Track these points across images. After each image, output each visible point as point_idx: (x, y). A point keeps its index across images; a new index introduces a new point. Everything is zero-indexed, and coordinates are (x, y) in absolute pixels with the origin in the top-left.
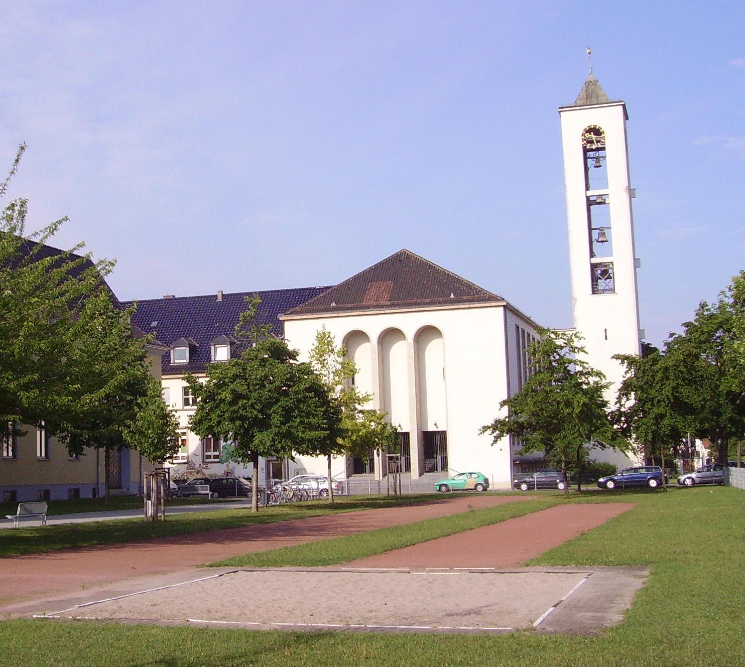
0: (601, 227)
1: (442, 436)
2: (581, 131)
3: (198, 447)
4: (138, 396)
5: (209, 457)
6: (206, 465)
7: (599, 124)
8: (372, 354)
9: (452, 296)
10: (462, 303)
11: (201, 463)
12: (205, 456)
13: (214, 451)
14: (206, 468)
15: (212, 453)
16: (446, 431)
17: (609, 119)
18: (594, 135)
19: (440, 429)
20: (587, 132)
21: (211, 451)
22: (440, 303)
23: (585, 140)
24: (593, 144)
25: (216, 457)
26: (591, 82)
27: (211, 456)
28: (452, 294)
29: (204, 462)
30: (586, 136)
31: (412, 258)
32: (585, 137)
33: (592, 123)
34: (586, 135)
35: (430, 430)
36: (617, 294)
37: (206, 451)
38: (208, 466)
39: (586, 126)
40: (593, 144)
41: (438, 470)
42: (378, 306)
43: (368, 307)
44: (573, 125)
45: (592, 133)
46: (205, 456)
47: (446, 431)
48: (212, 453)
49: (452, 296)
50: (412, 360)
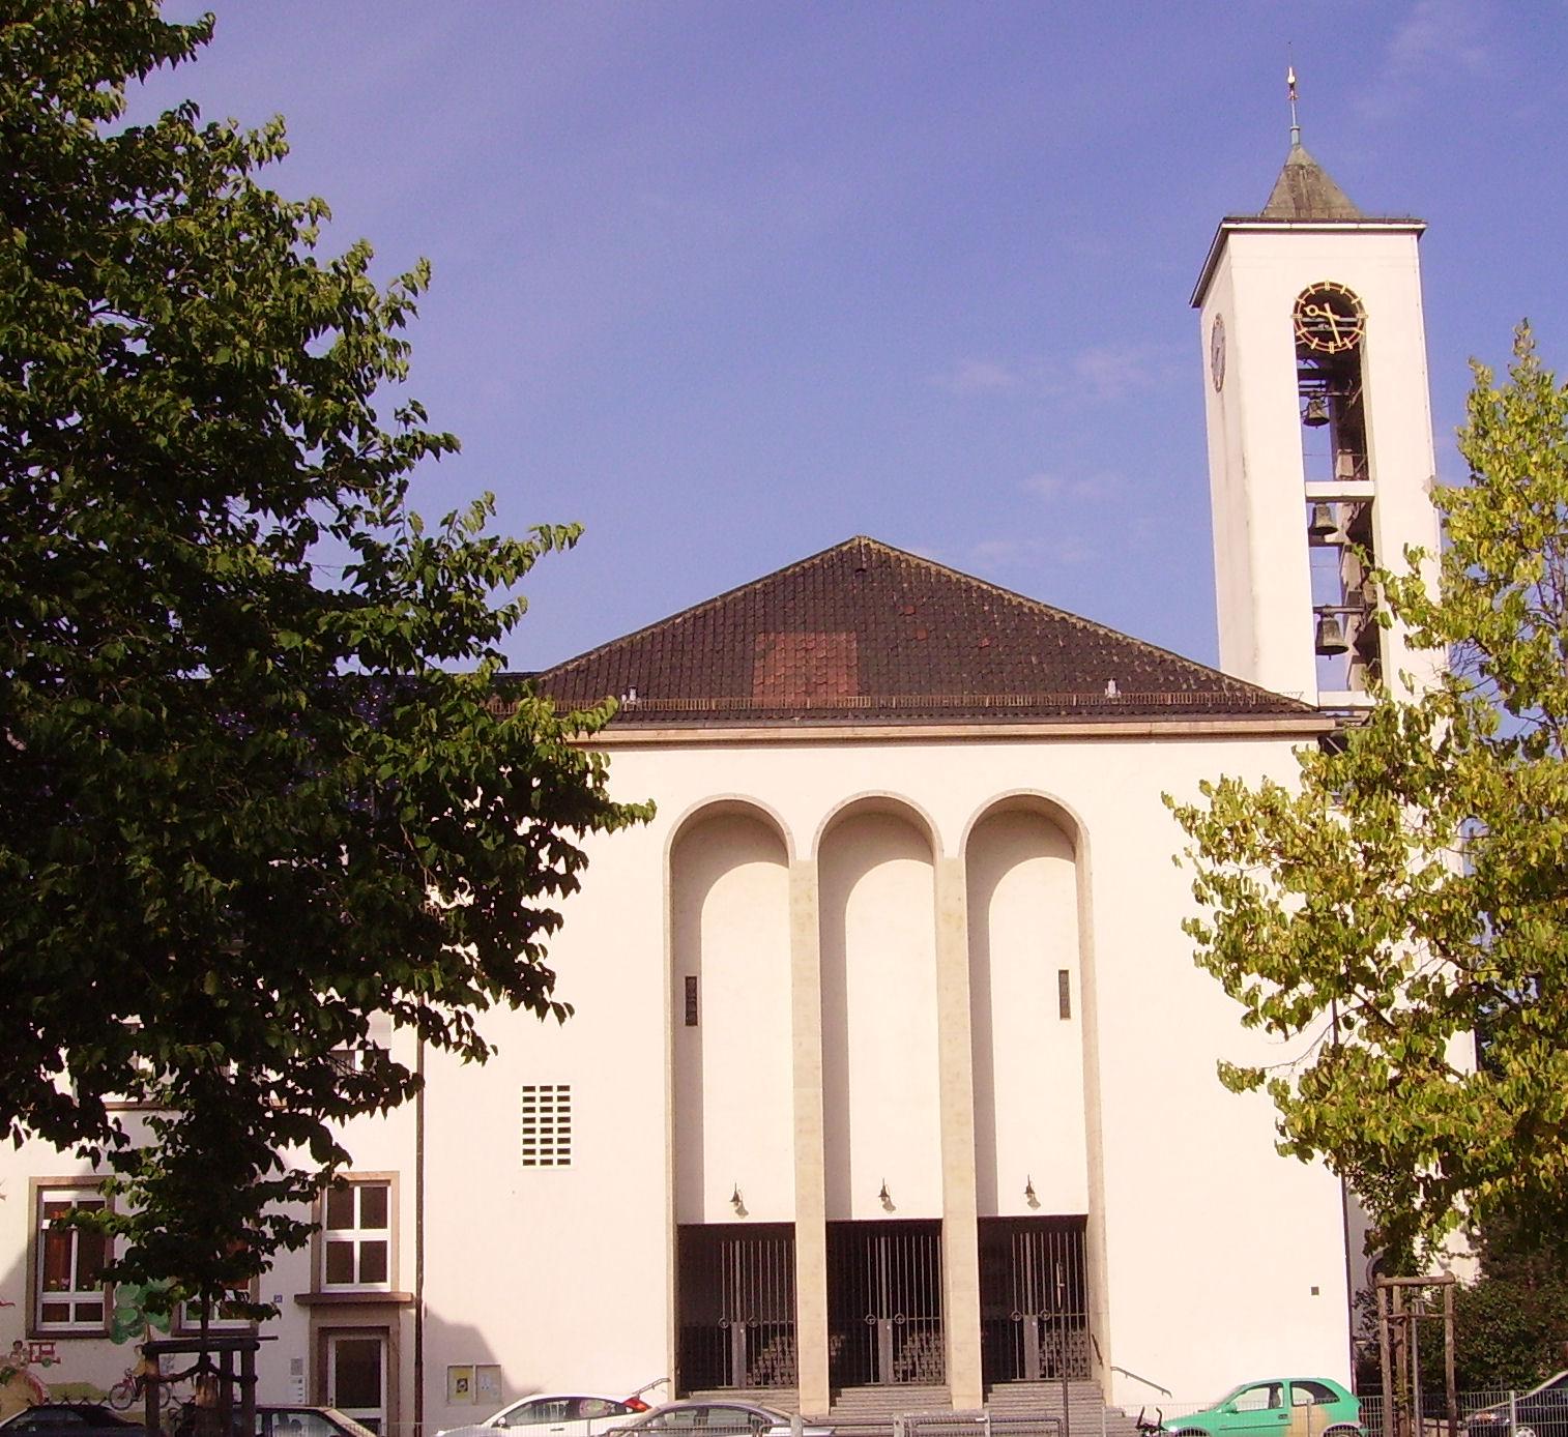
0: (1327, 607)
1: (1066, 1239)
2: (1292, 296)
3: (13, 1273)
4: (59, 266)
5: (58, 1312)
6: (48, 1348)
7: (1347, 282)
8: (795, 900)
9: (1111, 690)
10: (1162, 717)
11: (22, 1338)
12: (40, 1307)
13: (79, 1288)
14: (47, 1360)
15: (73, 1297)
16: (792, 1226)
17: (1383, 274)
18: (1334, 313)
19: (905, 1211)
20: (1310, 300)
21: (68, 1288)
22: (1074, 713)
23: (1306, 324)
24: (1332, 376)
25: (87, 1312)
26: (1302, 167)
27: (67, 1306)
28: (1112, 684)
29: (34, 1334)
30: (1309, 313)
31: (903, 565)
32: (1305, 314)
33: (1327, 276)
34: (1307, 309)
35: (1004, 1211)
36: (563, 1012)
37: (47, 1288)
38: (52, 1352)
39: (1307, 282)
40: (1332, 376)
41: (1027, 1374)
42: (814, 713)
43: (783, 715)
44: (1266, 277)
45: (1327, 306)
46: (40, 1307)
47: (792, 1226)
48: (73, 1297)
49: (1111, 690)
50: (959, 928)
